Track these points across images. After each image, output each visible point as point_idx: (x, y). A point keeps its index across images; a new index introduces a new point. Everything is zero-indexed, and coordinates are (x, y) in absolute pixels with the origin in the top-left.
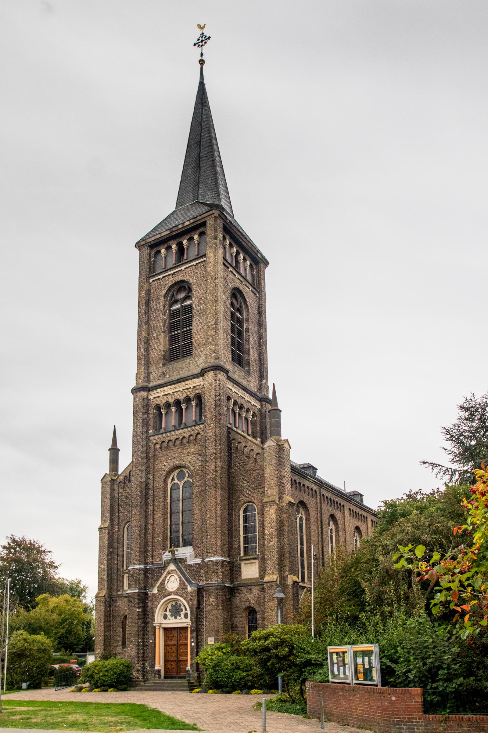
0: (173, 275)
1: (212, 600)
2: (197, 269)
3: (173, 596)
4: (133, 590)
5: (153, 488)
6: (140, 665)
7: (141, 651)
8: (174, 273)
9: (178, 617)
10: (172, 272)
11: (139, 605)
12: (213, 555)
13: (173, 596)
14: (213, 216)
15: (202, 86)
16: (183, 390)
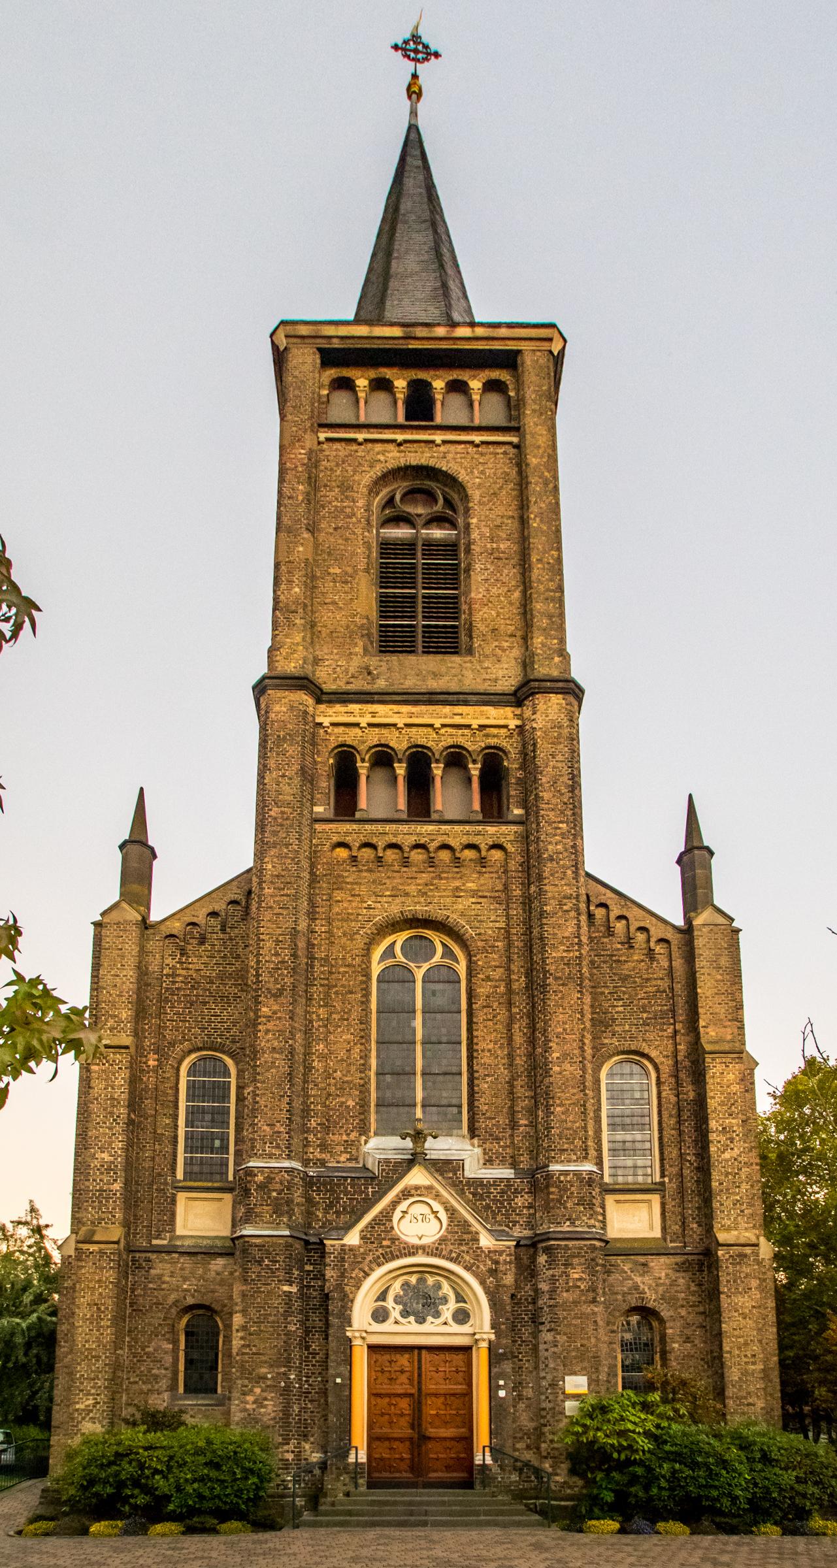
0: (400, 445)
1: (576, 1276)
2: (482, 454)
5: (542, 939)
6: (291, 1447)
7: (296, 1408)
8: (406, 441)
9: (430, 1319)
10: (400, 437)
12: (574, 1158)
14: (545, 346)
15: (413, 147)
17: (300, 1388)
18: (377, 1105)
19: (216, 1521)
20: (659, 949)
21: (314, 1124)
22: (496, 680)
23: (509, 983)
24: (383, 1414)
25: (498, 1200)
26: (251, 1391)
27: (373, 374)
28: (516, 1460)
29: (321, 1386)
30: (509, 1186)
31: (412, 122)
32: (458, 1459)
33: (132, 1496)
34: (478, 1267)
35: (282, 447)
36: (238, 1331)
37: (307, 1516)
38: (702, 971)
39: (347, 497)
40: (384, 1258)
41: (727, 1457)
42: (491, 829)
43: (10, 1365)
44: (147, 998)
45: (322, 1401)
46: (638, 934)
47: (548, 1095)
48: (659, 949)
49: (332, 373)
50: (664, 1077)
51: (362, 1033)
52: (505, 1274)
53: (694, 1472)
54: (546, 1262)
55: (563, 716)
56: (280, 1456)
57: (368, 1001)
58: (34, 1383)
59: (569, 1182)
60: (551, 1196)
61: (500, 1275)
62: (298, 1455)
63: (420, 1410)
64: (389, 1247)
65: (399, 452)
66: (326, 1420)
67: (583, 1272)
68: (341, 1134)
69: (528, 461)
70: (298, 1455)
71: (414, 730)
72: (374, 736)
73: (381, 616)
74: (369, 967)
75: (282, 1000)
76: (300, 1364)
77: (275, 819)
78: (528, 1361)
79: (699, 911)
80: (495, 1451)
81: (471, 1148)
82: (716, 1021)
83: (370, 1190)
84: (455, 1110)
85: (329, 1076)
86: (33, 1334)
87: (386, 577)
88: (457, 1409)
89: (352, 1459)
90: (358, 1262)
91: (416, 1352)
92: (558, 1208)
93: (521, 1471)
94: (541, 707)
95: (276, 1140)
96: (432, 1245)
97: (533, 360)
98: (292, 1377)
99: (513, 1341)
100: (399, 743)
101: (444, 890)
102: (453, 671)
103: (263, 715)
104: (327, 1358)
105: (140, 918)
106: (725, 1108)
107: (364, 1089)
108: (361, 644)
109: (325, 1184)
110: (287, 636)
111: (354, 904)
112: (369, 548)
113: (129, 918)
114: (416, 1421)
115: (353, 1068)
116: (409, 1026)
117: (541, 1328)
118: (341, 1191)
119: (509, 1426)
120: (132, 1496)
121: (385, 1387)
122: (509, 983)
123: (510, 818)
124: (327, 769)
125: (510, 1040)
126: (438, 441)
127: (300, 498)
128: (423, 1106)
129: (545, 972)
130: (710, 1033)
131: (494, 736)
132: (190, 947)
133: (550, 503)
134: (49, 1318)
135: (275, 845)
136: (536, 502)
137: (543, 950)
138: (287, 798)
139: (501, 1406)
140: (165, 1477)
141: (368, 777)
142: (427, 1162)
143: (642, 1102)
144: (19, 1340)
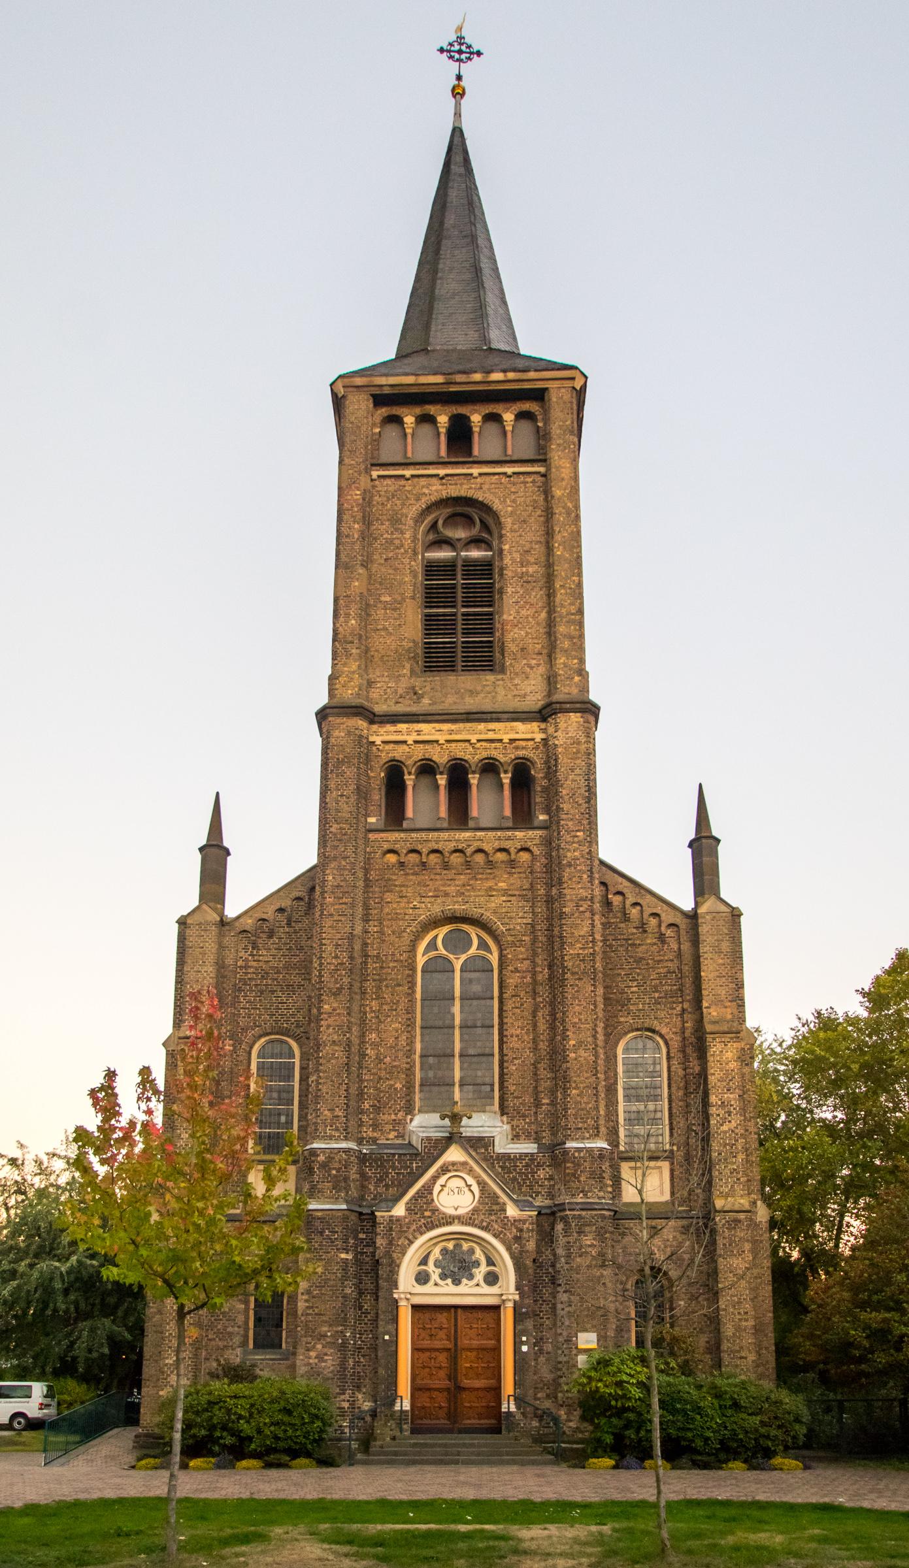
0: (442, 478)
1: (589, 1243)
3: (456, 1228)
4: (328, 1203)
5: (561, 937)
6: (347, 1397)
8: (447, 475)
9: (464, 1281)
10: (442, 472)
11: (346, 1241)
12: (587, 1135)
13: (456, 1228)
14: (569, 384)
15: (457, 134)
16: (479, 741)
17: (354, 1344)
18: (421, 1085)
19: (288, 1458)
20: (669, 933)
21: (367, 1106)
22: (525, 696)
23: (534, 974)
24: (424, 1367)
26: (314, 1347)
27: (418, 411)
28: (537, 1409)
29: (372, 1342)
30: (532, 1160)
31: (456, 125)
33: (221, 1438)
35: (340, 488)
36: (302, 1294)
37: (359, 1456)
38: (706, 956)
39: (396, 530)
41: (702, 1404)
42: (519, 834)
43: (49, 1312)
44: (224, 989)
45: (373, 1356)
46: (651, 919)
47: (566, 1079)
48: (669, 933)
49: (384, 411)
50: (673, 1052)
51: (409, 1022)
53: (673, 1416)
55: (581, 733)
57: (414, 992)
58: (72, 1332)
60: (567, 1171)
61: (524, 1242)
62: (353, 1404)
64: (430, 1217)
65: (443, 485)
66: (376, 1372)
67: (594, 1239)
69: (554, 493)
70: (353, 1404)
71: (453, 745)
72: (419, 753)
73: (426, 634)
74: (415, 961)
75: (341, 997)
76: (355, 1323)
77: (335, 834)
79: (706, 896)
80: (519, 1400)
81: (501, 1124)
82: (718, 1002)
84: (488, 1088)
85: (381, 1061)
86: (72, 1277)
87: (432, 596)
88: (489, 1362)
89: (397, 1407)
91: (453, 1310)
94: (562, 725)
97: (558, 395)
98: (348, 1334)
99: (535, 1301)
100: (440, 757)
101: (479, 890)
102: (487, 688)
103: (325, 735)
104: (377, 1317)
105: (218, 919)
106: (725, 1084)
107: (410, 1072)
108: (408, 666)
109: (376, 1161)
110: (345, 665)
111: (402, 905)
112: (415, 577)
113: (209, 918)
114: (453, 1375)
115: (400, 1054)
116: (449, 1012)
117: (559, 1289)
119: (531, 1378)
120: (221, 1438)
122: (534, 974)
123: (536, 824)
124: (378, 782)
125: (535, 1026)
126: (476, 474)
127: (356, 536)
128: (461, 1085)
129: (564, 967)
130: (712, 1012)
131: (523, 748)
132: (260, 941)
133: (572, 532)
134: (89, 1262)
135: (335, 858)
136: (559, 532)
137: (562, 948)
138: (344, 815)
140: (248, 1422)
141: (413, 435)
142: (463, 1140)
143: (655, 1074)
144: (58, 1285)
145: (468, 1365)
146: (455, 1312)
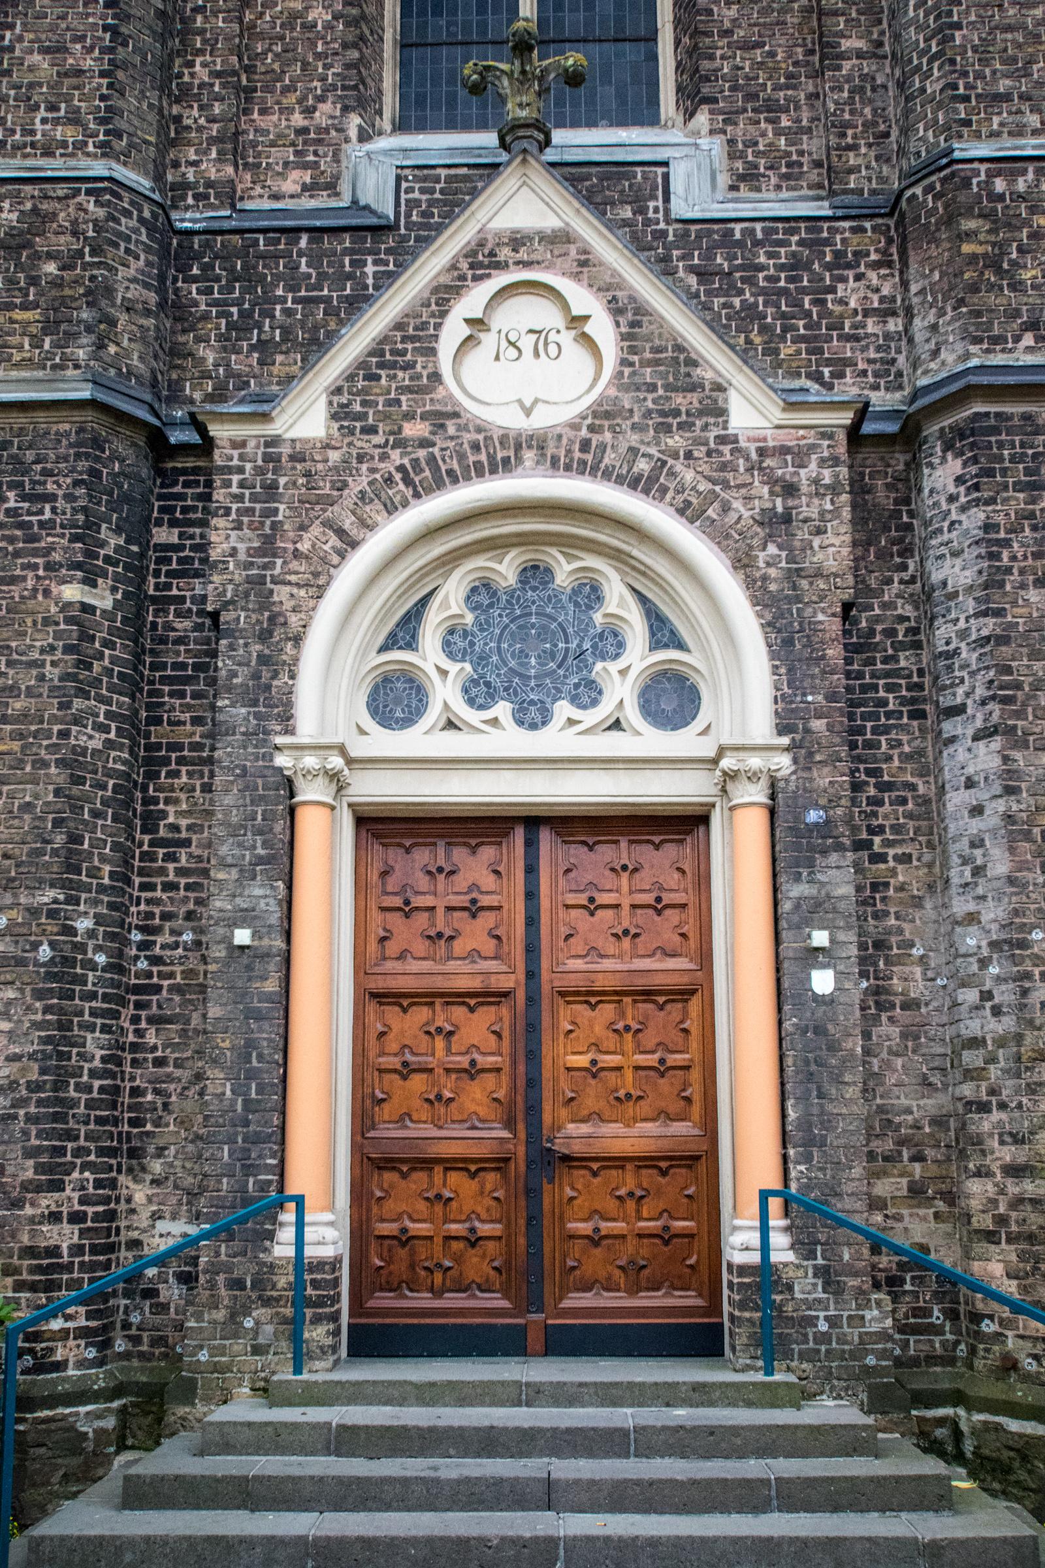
7: (95, 1045)
9: (563, 709)
11: (86, 534)
21: (202, 73)
24: (406, 1071)
25: (785, 292)
32: (666, 1237)
34: (726, 508)
40: (407, 481)
52: (820, 531)
54: (959, 480)
56: (25, 1239)
59: (1021, 197)
61: (803, 534)
63: (533, 1056)
64: (425, 443)
68: (291, 111)
78: (905, 859)
83: (370, 269)
89: (283, 1248)
90: (319, 500)
91: (519, 834)
92: (991, 287)
93: (893, 1283)
95: (68, 100)
96: (568, 433)
98: (83, 924)
109: (226, 257)
117: (949, 727)
118: (278, 277)
121: (415, 966)
139: (820, 1030)
145: (582, 1061)
146: (531, 844)
